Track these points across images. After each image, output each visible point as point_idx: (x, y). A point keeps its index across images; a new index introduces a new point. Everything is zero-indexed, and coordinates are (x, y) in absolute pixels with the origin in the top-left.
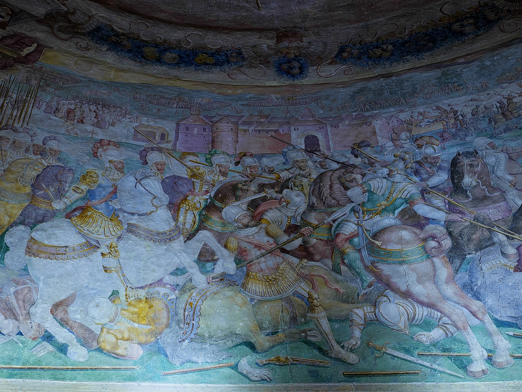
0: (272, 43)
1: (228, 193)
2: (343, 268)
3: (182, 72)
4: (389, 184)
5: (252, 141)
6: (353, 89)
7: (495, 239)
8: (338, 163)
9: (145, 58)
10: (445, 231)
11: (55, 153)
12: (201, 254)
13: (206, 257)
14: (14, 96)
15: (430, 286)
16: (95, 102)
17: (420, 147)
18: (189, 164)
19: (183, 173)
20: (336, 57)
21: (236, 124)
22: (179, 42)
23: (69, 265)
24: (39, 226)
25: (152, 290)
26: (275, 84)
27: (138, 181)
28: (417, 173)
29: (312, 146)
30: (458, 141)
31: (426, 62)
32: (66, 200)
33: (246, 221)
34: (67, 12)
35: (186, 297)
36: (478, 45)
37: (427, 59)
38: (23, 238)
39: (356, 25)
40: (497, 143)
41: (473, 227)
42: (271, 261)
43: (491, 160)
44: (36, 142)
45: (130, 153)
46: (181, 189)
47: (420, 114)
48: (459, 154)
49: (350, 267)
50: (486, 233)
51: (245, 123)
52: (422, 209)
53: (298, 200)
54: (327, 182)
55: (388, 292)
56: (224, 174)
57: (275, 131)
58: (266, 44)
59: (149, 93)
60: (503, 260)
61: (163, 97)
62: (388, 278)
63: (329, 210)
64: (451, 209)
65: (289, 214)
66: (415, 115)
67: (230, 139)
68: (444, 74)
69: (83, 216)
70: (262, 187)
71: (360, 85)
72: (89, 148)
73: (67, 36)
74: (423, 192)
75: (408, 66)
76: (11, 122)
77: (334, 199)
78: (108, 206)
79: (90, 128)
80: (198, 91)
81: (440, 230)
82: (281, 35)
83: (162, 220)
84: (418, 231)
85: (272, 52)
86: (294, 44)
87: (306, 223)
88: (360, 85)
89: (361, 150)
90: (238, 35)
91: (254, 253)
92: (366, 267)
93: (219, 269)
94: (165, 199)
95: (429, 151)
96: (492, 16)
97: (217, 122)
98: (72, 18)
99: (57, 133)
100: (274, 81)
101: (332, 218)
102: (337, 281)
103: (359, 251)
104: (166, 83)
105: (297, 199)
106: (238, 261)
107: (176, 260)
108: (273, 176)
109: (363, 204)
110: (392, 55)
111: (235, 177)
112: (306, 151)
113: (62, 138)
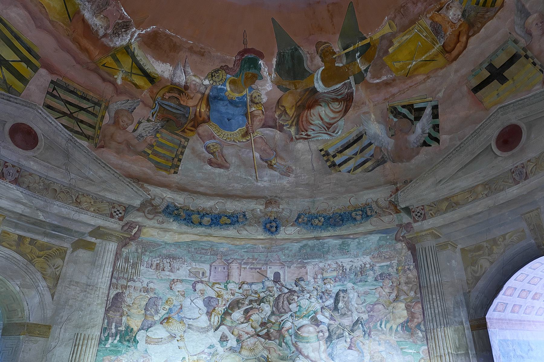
0: (262, 207)
1: (235, 305)
2: (283, 344)
3: (212, 231)
4: (309, 302)
5: (248, 275)
6: (301, 244)
7: (344, 334)
8: (288, 289)
9: (193, 223)
10: (327, 328)
11: (153, 290)
12: (221, 338)
13: (223, 339)
14: (132, 261)
15: (317, 353)
16: (169, 257)
17: (325, 284)
18: (216, 289)
19: (213, 295)
20: (295, 221)
21: (240, 264)
22: (211, 208)
23: (163, 347)
24: (149, 330)
25: (199, 356)
26: (262, 237)
27: (192, 301)
28: (321, 298)
29: (277, 276)
30: (341, 283)
31: (337, 233)
32: (159, 315)
33: (242, 320)
34: (151, 199)
35: (214, 358)
36: (361, 229)
37: (338, 231)
38: (144, 336)
39: (308, 200)
40: (356, 287)
41: (338, 328)
42: (253, 340)
43: (351, 296)
44: (144, 286)
45: (188, 286)
46: (212, 304)
47: (329, 265)
48: (340, 290)
49: (286, 344)
50: (342, 331)
51: (245, 263)
52: (320, 317)
53: (267, 308)
54: (281, 300)
55: (300, 356)
56: (233, 294)
57: (260, 269)
58: (259, 207)
59: (196, 247)
60: (345, 344)
61: (203, 249)
62: (301, 349)
63: (281, 315)
64: (332, 318)
65: (263, 317)
66: (326, 265)
67: (236, 274)
68: (343, 243)
69: (167, 322)
70: (251, 302)
71: (304, 242)
72: (168, 285)
73: (152, 216)
74: (322, 308)
75: (328, 234)
76: (132, 276)
77: (283, 309)
78: (179, 315)
79: (168, 273)
80: (221, 243)
81: (324, 327)
82: (270, 202)
83: (203, 321)
84: (316, 327)
85: (262, 215)
86: (275, 210)
87: (269, 321)
88: (304, 242)
89: (299, 282)
90: (245, 201)
91: (245, 336)
92: (293, 344)
93: (229, 345)
94: (205, 310)
95: (328, 286)
96: (369, 213)
97: (231, 263)
98: (154, 202)
99: (153, 279)
100: (261, 235)
101: (281, 319)
102: (280, 350)
103: (291, 336)
104: (205, 239)
105: (267, 309)
106: (238, 341)
107: (210, 341)
108: (257, 296)
109: (296, 313)
110: (323, 225)
111: (238, 296)
112: (274, 281)
113: (155, 281)
